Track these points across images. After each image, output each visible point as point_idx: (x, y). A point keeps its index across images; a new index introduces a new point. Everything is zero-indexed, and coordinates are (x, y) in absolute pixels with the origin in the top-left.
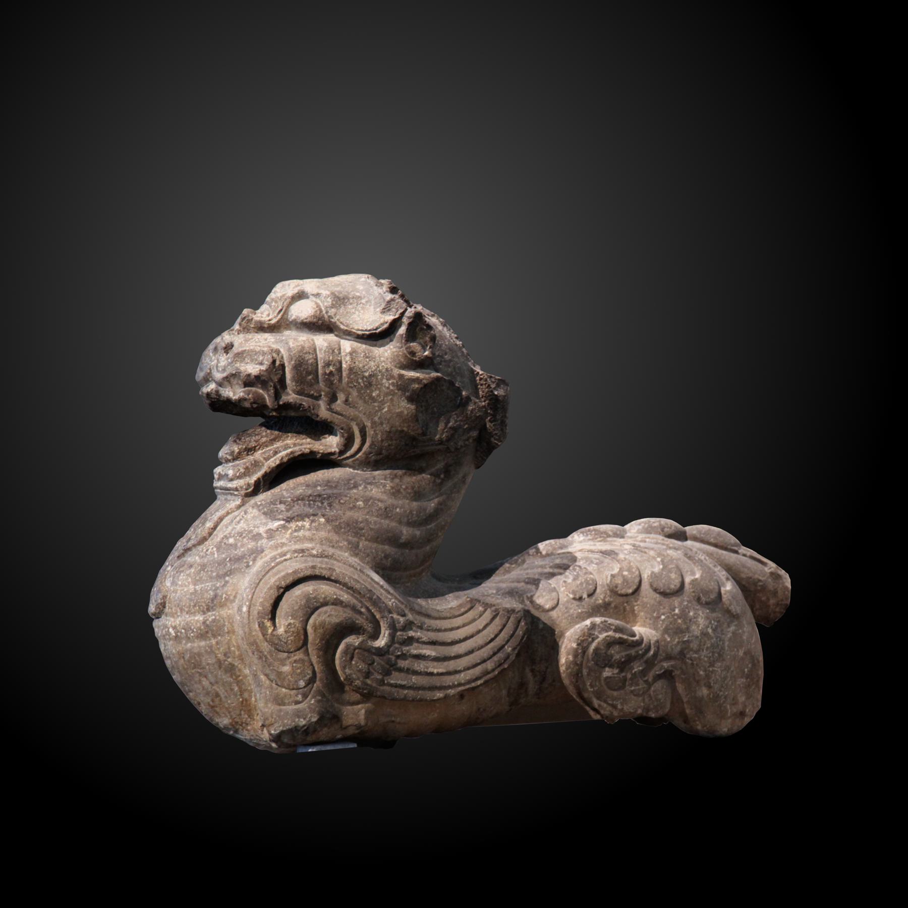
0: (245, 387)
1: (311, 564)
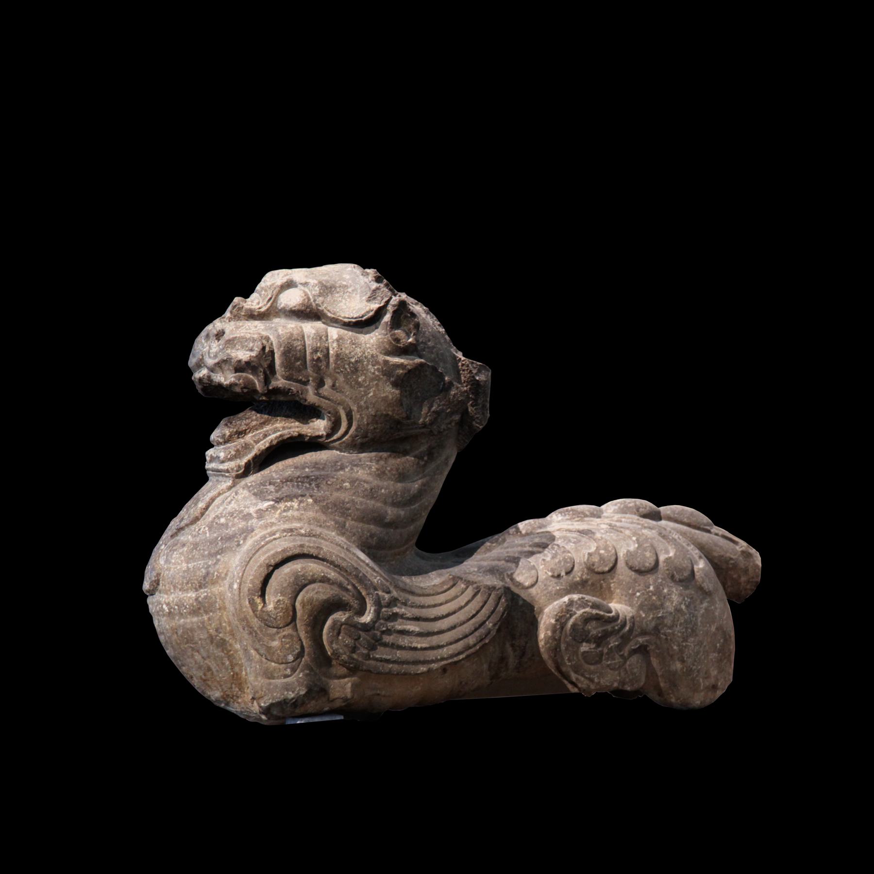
0: (236, 372)
1: (299, 543)
